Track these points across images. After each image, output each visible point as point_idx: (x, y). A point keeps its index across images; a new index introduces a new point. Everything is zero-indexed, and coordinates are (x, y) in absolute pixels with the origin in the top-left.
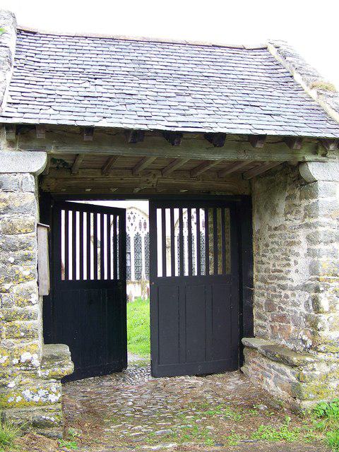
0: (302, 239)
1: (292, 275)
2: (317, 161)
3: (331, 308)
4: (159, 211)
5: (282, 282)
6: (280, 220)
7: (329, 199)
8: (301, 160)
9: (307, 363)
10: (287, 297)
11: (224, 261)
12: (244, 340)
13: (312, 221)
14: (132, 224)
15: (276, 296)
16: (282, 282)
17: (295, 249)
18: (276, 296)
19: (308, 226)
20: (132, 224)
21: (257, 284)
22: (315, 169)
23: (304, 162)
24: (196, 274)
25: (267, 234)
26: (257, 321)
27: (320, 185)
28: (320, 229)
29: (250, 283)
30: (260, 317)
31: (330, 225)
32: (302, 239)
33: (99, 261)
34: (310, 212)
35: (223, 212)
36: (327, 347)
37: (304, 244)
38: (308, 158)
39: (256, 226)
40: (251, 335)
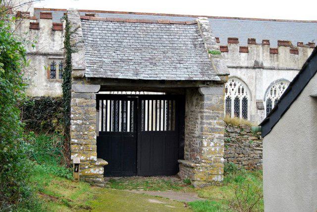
0: (199, 117)
1: (196, 132)
2: (204, 87)
3: (207, 145)
4: (101, 101)
5: (194, 135)
6: (194, 108)
7: (209, 102)
8: (197, 86)
9: (197, 166)
10: (194, 141)
11: (172, 123)
12: (180, 161)
13: (203, 110)
14: (233, 90)
15: (191, 141)
16: (194, 135)
17: (197, 121)
18: (191, 141)
19: (201, 112)
20: (233, 90)
21: (186, 135)
22: (203, 90)
23: (199, 87)
24: (120, 101)
25: (190, 113)
26: (186, 153)
27: (205, 96)
28: (204, 114)
29: (183, 134)
30: (187, 151)
31: (209, 113)
32: (199, 117)
33: (104, 122)
34: (202, 107)
35: (172, 103)
36: (206, 161)
37: (200, 120)
38: (200, 86)
39: (187, 110)
40: (183, 159)
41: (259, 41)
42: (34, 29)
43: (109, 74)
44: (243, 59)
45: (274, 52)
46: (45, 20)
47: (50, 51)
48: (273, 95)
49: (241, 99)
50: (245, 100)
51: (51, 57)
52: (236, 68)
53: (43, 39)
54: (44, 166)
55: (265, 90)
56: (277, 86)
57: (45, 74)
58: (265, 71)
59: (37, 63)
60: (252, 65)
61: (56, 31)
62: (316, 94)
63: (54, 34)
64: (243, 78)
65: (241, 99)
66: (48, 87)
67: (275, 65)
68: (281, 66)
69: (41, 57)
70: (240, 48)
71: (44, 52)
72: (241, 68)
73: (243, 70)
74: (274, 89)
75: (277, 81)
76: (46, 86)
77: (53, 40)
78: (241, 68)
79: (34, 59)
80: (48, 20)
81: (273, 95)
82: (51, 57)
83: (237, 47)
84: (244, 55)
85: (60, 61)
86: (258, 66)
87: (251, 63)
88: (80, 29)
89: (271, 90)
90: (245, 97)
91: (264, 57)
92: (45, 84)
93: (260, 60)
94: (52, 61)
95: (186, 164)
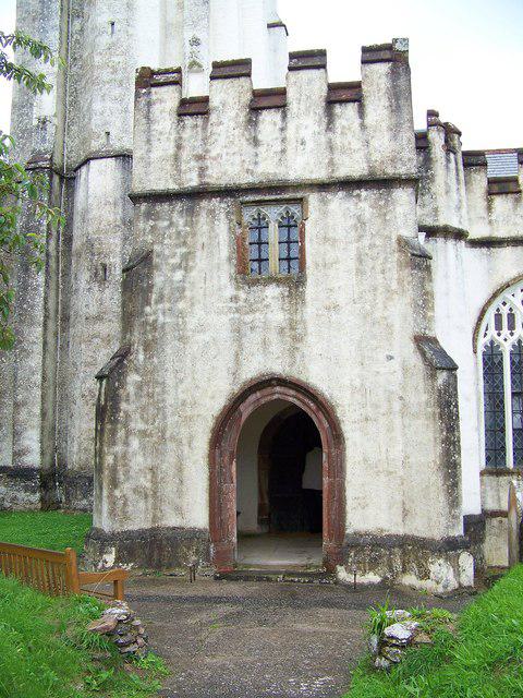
42: (191, 115)
46: (228, 81)
47: (245, 180)
48: (505, 331)
51: (250, 198)
53: (222, 140)
54: (141, 426)
57: (230, 259)
59: (203, 219)
61: (265, 113)
62: (521, 233)
63: (256, 123)
66: (241, 303)
69: (215, 201)
70: (491, 182)
71: (223, 182)
74: (505, 311)
76: (235, 299)
77: (256, 142)
79: (191, 212)
80: (236, 82)
81: (505, 331)
82: (250, 198)
85: (281, 209)
88: (382, 411)
89: (498, 317)
90: (492, 342)
92: (230, 291)
94: (253, 211)
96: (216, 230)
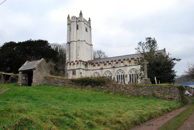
41: (114, 61)
43: (90, 108)
44: (122, 65)
45: (130, 61)
49: (118, 75)
50: (124, 75)
52: (120, 67)
55: (116, 72)
56: (132, 71)
58: (128, 67)
60: (100, 68)
64: (111, 71)
65: (118, 75)
67: (131, 65)
68: (132, 65)
72: (122, 67)
73: (90, 71)
75: (131, 69)
78: (122, 67)
83: (97, 65)
84: (122, 63)
86: (126, 66)
87: (124, 65)
91: (126, 63)
93: (126, 64)
95: (161, 118)
96: (71, 72)
